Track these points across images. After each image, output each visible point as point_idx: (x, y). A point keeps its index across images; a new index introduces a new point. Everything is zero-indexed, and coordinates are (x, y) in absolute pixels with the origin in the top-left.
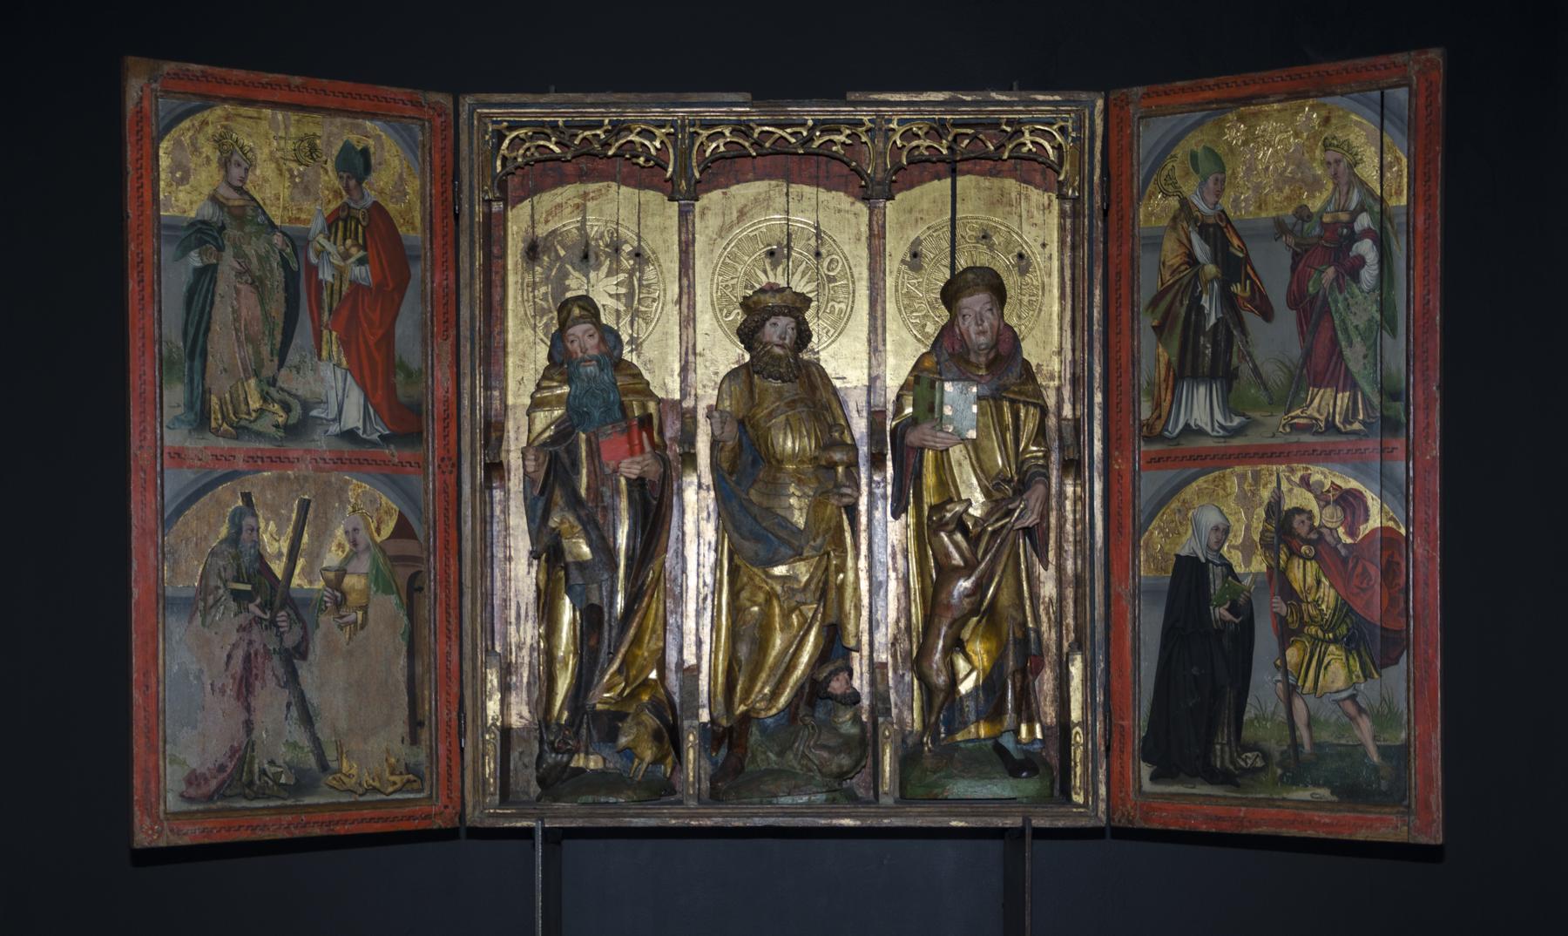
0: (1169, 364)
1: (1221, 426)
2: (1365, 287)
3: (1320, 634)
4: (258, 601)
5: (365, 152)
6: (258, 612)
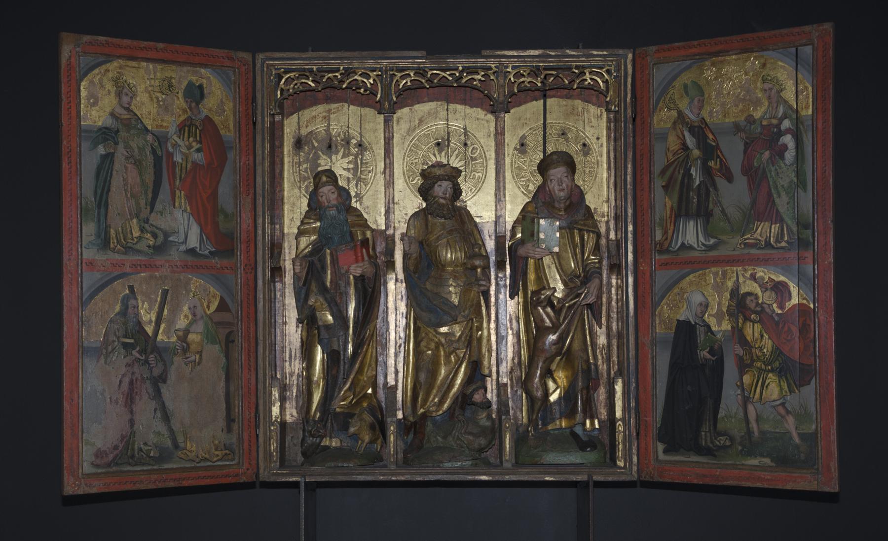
1: (703, 244)
2: (787, 163)
3: (763, 366)
4: (138, 349)
5: (201, 87)
6: (138, 355)
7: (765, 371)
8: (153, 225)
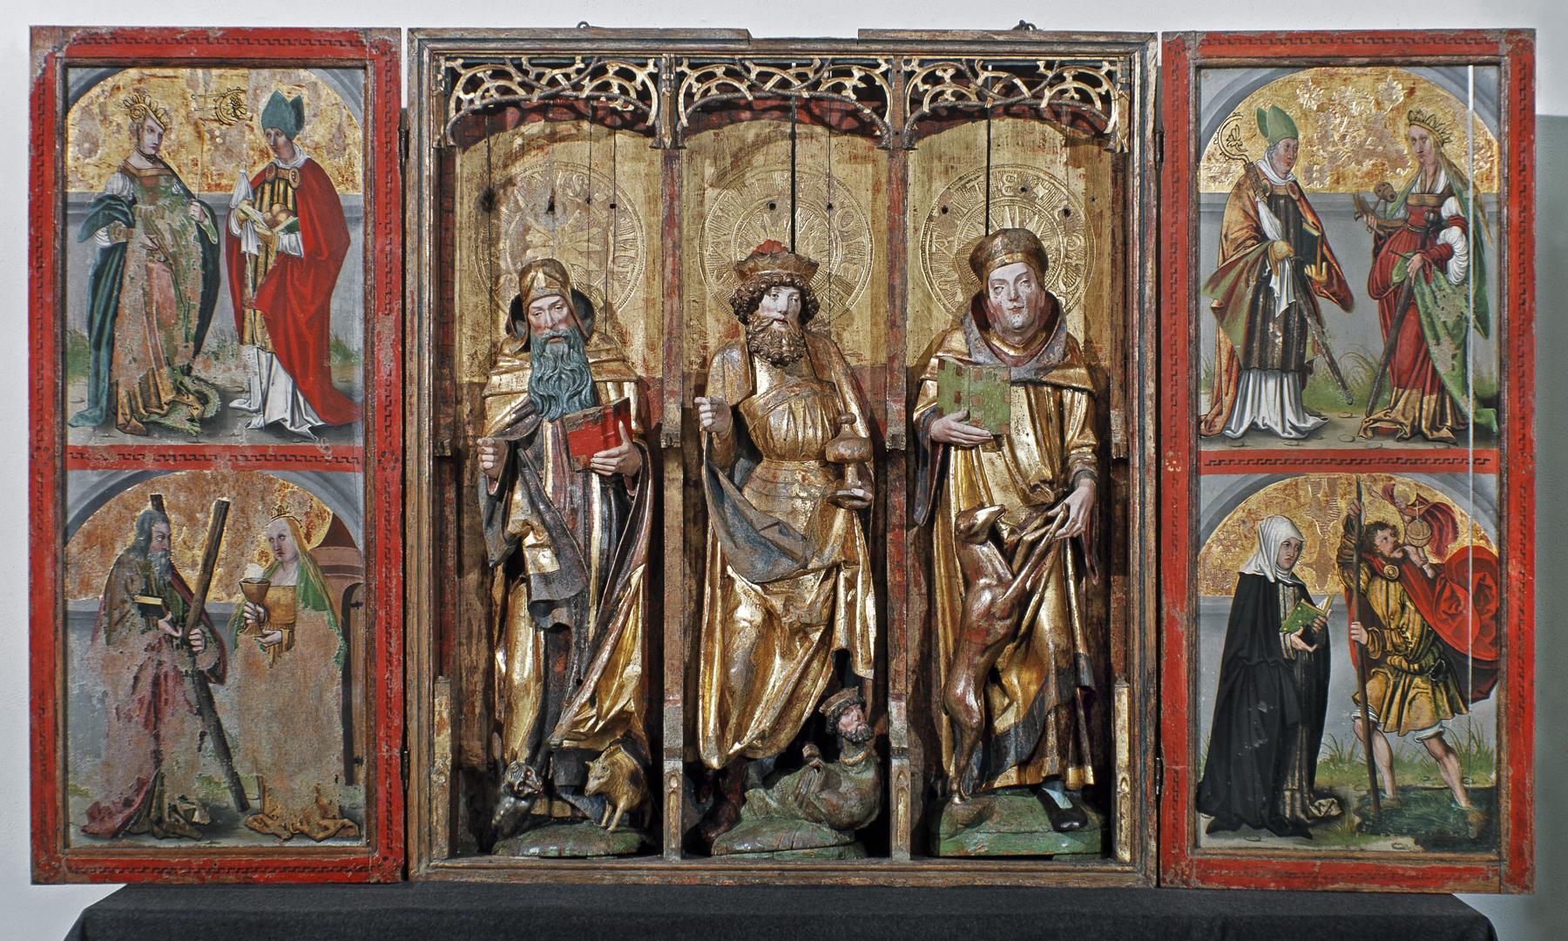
0: (1232, 353)
1: (1294, 427)
2: (1453, 279)
3: (1404, 664)
4: (169, 616)
5: (297, 105)
6: (169, 629)
7: (1407, 672)
8: (198, 378)
